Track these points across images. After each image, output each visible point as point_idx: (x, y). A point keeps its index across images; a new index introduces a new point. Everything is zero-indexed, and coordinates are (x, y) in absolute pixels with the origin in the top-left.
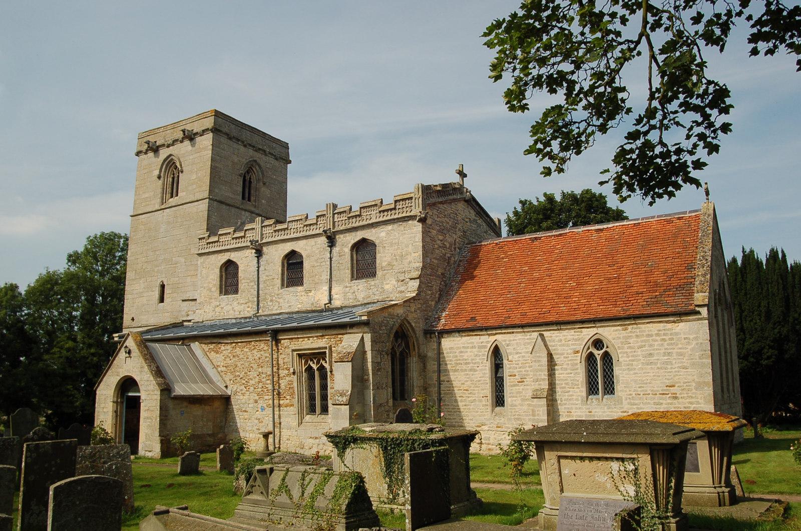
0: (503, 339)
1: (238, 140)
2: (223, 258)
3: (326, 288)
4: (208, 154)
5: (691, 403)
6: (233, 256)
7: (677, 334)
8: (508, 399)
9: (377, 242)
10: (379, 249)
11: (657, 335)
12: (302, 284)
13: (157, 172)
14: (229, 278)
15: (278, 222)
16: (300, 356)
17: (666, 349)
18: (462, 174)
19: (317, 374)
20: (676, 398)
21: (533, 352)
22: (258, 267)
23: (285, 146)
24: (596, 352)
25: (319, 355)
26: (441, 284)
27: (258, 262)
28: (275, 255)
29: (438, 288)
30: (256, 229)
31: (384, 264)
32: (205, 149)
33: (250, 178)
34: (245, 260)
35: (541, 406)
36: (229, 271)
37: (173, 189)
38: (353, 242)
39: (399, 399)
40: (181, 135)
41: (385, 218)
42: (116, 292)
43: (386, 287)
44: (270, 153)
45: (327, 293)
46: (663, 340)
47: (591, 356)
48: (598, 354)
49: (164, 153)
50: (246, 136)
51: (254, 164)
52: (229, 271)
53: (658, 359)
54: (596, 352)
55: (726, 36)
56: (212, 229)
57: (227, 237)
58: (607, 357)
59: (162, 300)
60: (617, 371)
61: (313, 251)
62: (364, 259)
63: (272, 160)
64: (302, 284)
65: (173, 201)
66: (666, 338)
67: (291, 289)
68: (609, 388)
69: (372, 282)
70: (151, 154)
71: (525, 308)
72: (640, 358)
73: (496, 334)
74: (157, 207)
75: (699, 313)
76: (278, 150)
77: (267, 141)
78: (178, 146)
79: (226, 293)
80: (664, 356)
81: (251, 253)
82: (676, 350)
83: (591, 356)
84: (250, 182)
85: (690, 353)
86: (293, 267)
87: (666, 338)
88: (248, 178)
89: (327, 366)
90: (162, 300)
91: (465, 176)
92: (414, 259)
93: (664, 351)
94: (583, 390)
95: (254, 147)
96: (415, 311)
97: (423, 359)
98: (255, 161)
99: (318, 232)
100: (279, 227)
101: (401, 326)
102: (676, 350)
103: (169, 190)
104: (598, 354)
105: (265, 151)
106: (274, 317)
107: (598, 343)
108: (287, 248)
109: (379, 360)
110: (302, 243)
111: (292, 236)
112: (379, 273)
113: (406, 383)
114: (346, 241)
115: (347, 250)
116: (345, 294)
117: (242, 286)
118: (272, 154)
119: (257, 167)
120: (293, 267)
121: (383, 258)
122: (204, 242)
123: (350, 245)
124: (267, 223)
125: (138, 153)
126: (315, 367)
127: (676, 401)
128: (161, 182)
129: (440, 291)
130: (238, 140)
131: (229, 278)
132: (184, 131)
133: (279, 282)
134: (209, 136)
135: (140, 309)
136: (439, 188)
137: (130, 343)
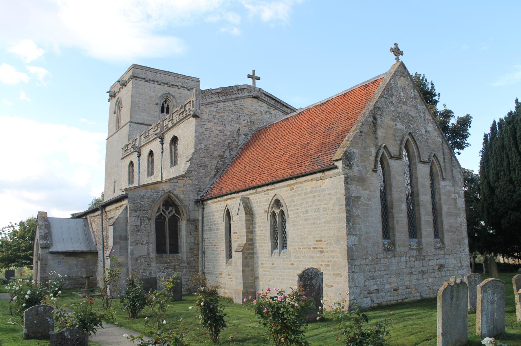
1: (154, 81)
5: (332, 257)
7: (323, 190)
11: (311, 192)
17: (316, 205)
18: (253, 77)
20: (322, 252)
21: (239, 214)
22: (139, 164)
26: (218, 163)
29: (214, 167)
33: (168, 105)
39: (168, 252)
44: (182, 87)
46: (314, 197)
47: (274, 214)
48: (277, 211)
50: (160, 78)
51: (169, 95)
53: (311, 216)
63: (185, 91)
66: (316, 194)
72: (301, 214)
73: (227, 200)
75: (336, 167)
77: (180, 79)
80: (315, 212)
82: (322, 206)
83: (274, 214)
84: (276, 108)
85: (332, 208)
87: (316, 194)
88: (166, 106)
93: (314, 207)
95: (167, 84)
96: (184, 186)
97: (194, 223)
98: (169, 93)
101: (169, 197)
102: (322, 206)
104: (277, 211)
105: (177, 86)
107: (277, 203)
109: (139, 224)
113: (179, 241)
118: (184, 87)
119: (172, 97)
125: (109, 101)
127: (322, 255)
128: (116, 115)
129: (217, 170)
130: (154, 81)
136: (219, 91)
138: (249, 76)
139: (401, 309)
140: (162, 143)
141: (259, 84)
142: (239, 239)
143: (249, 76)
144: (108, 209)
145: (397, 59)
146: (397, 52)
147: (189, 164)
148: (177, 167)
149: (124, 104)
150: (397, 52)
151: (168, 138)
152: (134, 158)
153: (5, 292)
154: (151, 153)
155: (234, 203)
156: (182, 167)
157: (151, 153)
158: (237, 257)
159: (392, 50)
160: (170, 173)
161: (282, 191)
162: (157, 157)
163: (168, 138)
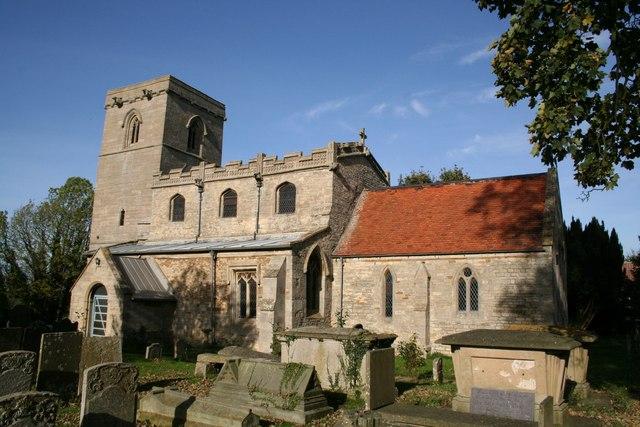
0: (392, 263)
2: (173, 192)
3: (255, 219)
4: (164, 109)
6: (180, 190)
8: (395, 312)
9: (297, 185)
10: (298, 191)
12: (235, 215)
13: (121, 123)
14: (178, 208)
15: (217, 167)
16: (235, 271)
18: (363, 136)
19: (248, 285)
23: (222, 107)
24: (465, 278)
25: (251, 272)
27: (201, 196)
28: (215, 191)
30: (203, 171)
31: (302, 203)
32: (161, 106)
34: (190, 193)
35: (421, 317)
36: (178, 204)
37: (135, 137)
38: (277, 184)
40: (141, 94)
41: (304, 167)
42: (86, 211)
43: (302, 220)
45: (255, 223)
48: (467, 280)
49: (126, 108)
52: (178, 204)
54: (465, 278)
55: (622, 166)
56: (165, 169)
57: (176, 175)
58: (474, 285)
59: (122, 223)
60: (481, 292)
61: (244, 188)
62: (287, 198)
64: (235, 215)
65: (134, 146)
67: (227, 219)
68: (475, 306)
69: (292, 216)
70: (116, 107)
71: (411, 242)
74: (120, 150)
76: (216, 110)
78: (139, 102)
79: (174, 220)
81: (194, 189)
86: (230, 205)
89: (256, 280)
90: (122, 223)
91: (366, 137)
92: (326, 199)
94: (455, 305)
99: (250, 174)
100: (218, 170)
103: (131, 137)
104: (467, 280)
106: (222, 206)
107: (468, 272)
108: (225, 186)
110: (237, 182)
111: (228, 177)
112: (298, 210)
114: (272, 183)
115: (273, 190)
116: (270, 224)
117: (187, 214)
120: (230, 205)
121: (301, 198)
122: (157, 179)
123: (275, 186)
124: (209, 166)
126: (247, 280)
131: (178, 208)
132: (144, 91)
133: (217, 213)
134: (164, 97)
135: (104, 230)
137: (100, 255)
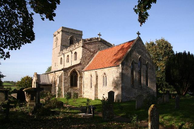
18: (99, 35)
107: (105, 74)
138: (98, 35)
139: (78, 79)
140: (72, 53)
141: (101, 37)
142: (94, 83)
143: (98, 35)
144: (56, 73)
145: (138, 36)
146: (138, 34)
147: (80, 61)
148: (76, 61)
149: (58, 39)
150: (138, 34)
151: (74, 52)
152: (62, 56)
153: (174, 61)
154: (68, 56)
155: (93, 73)
156: (78, 62)
157: (68, 56)
158: (93, 87)
159: (137, 33)
160: (75, 63)
161: (106, 70)
162: (70, 57)
163: (74, 52)
